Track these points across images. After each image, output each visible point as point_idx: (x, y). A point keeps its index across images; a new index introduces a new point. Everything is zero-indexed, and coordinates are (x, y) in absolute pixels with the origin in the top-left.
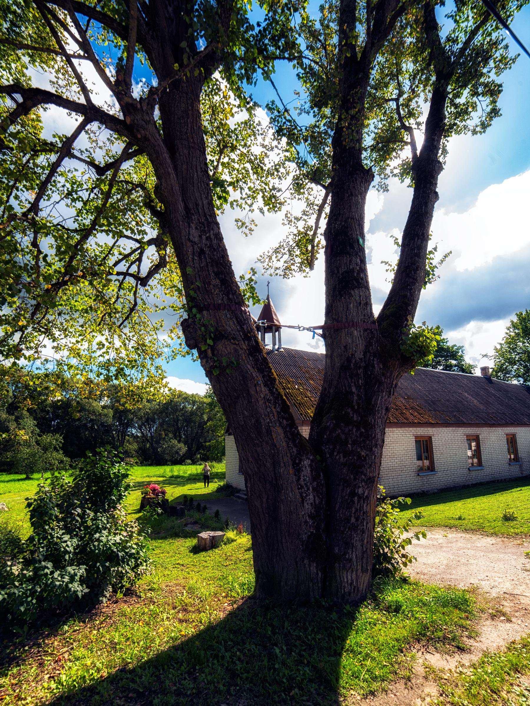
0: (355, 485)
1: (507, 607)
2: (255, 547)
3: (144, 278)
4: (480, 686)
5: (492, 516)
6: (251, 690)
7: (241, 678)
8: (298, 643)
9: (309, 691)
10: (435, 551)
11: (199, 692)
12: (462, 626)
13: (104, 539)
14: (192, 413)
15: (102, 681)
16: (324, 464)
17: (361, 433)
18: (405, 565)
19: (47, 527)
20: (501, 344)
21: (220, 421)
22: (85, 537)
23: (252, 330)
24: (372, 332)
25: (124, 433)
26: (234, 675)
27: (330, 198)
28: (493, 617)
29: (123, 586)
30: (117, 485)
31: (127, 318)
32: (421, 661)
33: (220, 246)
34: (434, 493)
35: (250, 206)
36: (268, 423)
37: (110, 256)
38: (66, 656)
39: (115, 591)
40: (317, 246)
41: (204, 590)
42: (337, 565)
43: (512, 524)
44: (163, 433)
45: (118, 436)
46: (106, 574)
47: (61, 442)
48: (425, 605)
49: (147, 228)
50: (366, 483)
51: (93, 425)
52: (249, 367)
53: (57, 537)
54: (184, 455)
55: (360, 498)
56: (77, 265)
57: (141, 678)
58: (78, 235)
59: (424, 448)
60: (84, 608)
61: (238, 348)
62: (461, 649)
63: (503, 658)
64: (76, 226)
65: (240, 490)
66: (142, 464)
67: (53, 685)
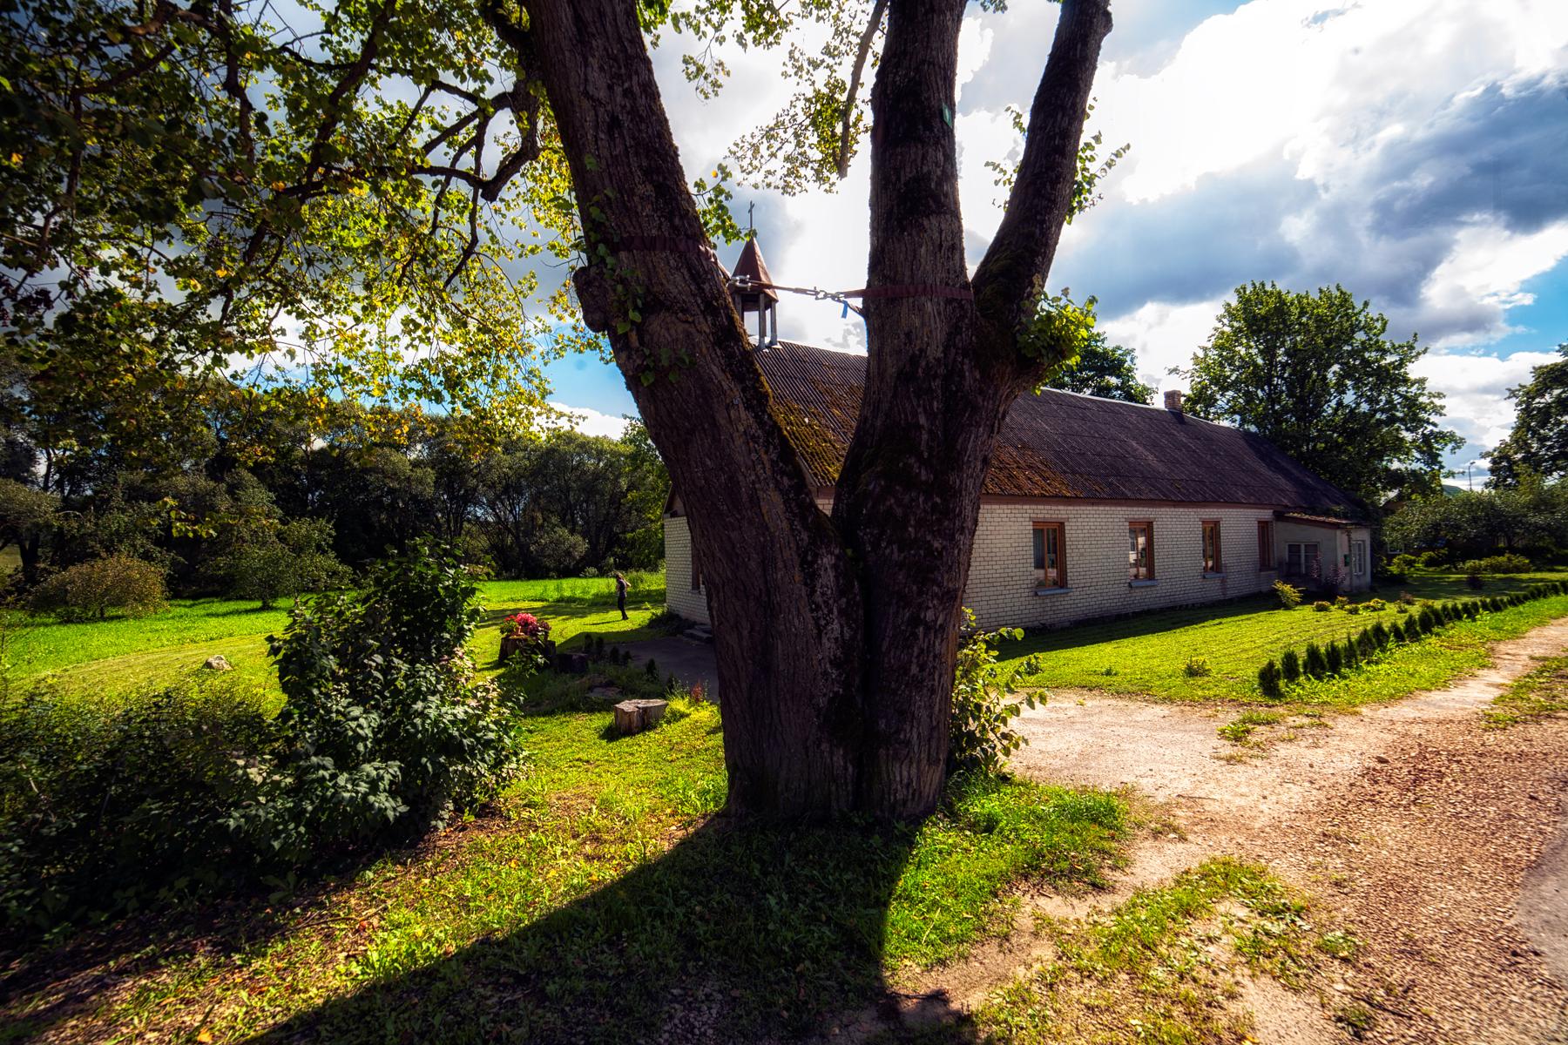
0: (920, 605)
1: (1182, 818)
2: (730, 725)
3: (488, 183)
4: (1125, 940)
5: (1166, 668)
6: (725, 966)
7: (706, 948)
8: (809, 889)
9: (830, 964)
10: (1060, 729)
11: (630, 973)
12: (1102, 851)
13: (433, 713)
14: (598, 476)
15: (447, 959)
16: (861, 565)
17: (935, 505)
18: (1007, 752)
19: (316, 692)
20: (1205, 349)
21: (653, 489)
22: (393, 710)
23: (721, 293)
24: (961, 307)
25: (460, 517)
26: (692, 944)
27: (885, 19)
28: (1156, 834)
29: (475, 800)
30: (454, 611)
31: (457, 271)
32: (1028, 909)
33: (654, 113)
34: (1063, 629)
35: (717, 29)
36: (753, 483)
37: (413, 132)
38: (375, 921)
39: (459, 810)
40: (855, 125)
41: (630, 804)
42: (882, 752)
43: (1200, 681)
44: (539, 515)
45: (448, 521)
46: (438, 783)
47: (330, 535)
48: (1039, 818)
49: (490, 66)
50: (941, 600)
51: (394, 501)
52: (715, 369)
53: (338, 712)
54: (582, 558)
55: (928, 628)
56: (338, 149)
57: (519, 952)
58: (333, 78)
59: (1050, 545)
60: (404, 839)
61: (693, 330)
62: (1099, 888)
63: (1167, 897)
64: (326, 56)
65: (693, 625)
66: (499, 577)
67: (356, 969)
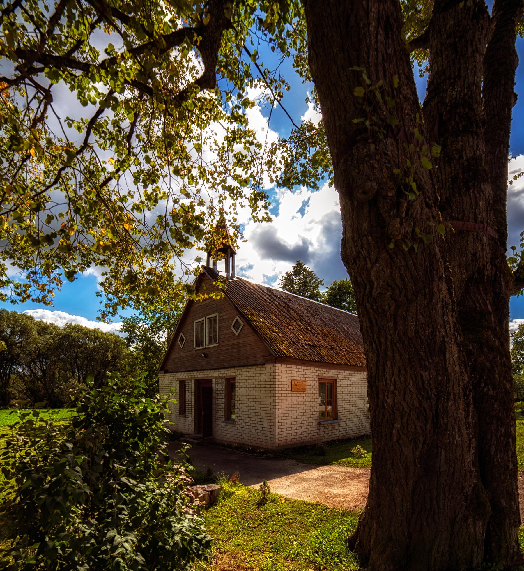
14: (94, 350)
36: (443, 337)
